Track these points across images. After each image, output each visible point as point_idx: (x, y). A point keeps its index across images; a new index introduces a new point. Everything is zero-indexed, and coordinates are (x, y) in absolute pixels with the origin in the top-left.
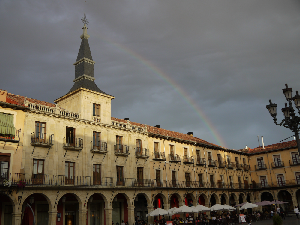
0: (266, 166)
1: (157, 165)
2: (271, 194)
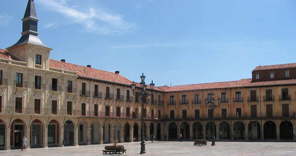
0: (176, 102)
2: (176, 124)
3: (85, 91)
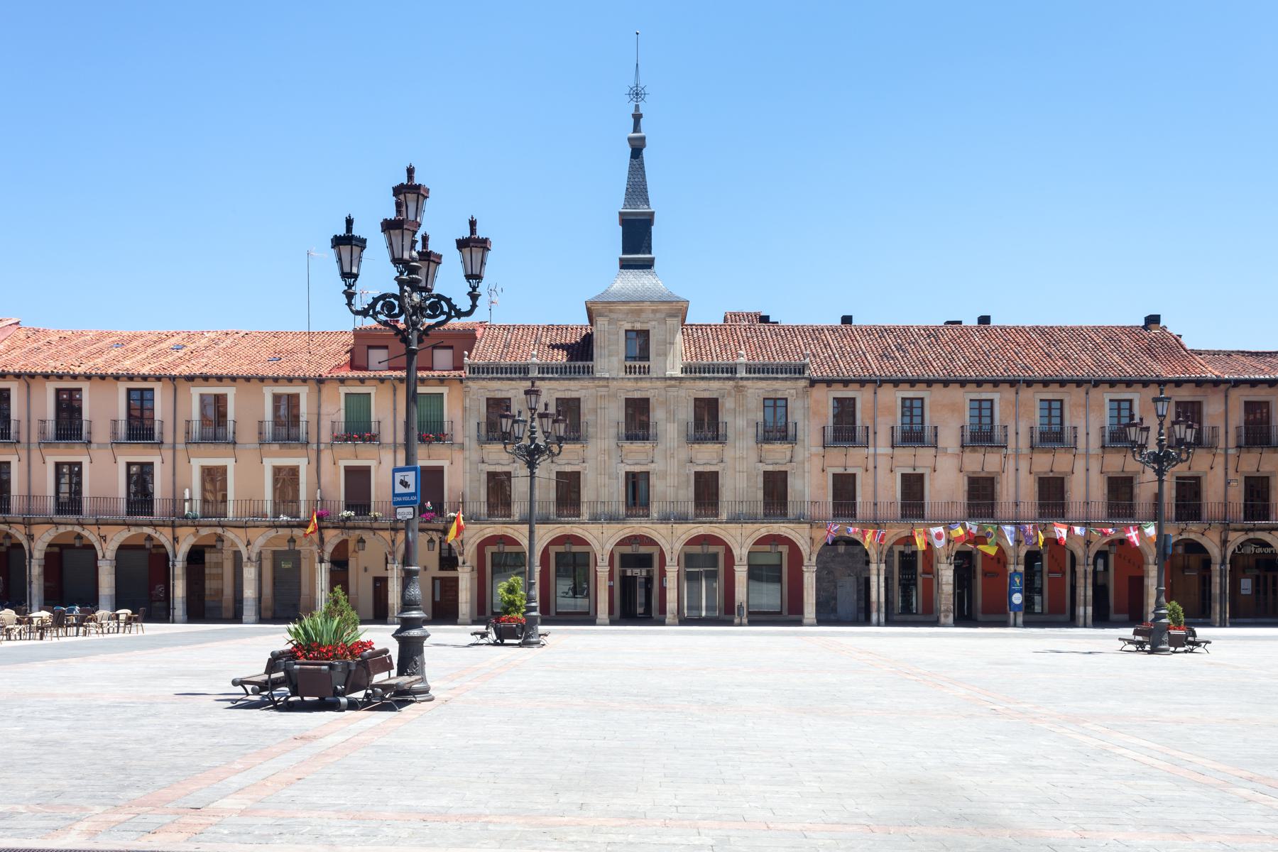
1: (1044, 463)
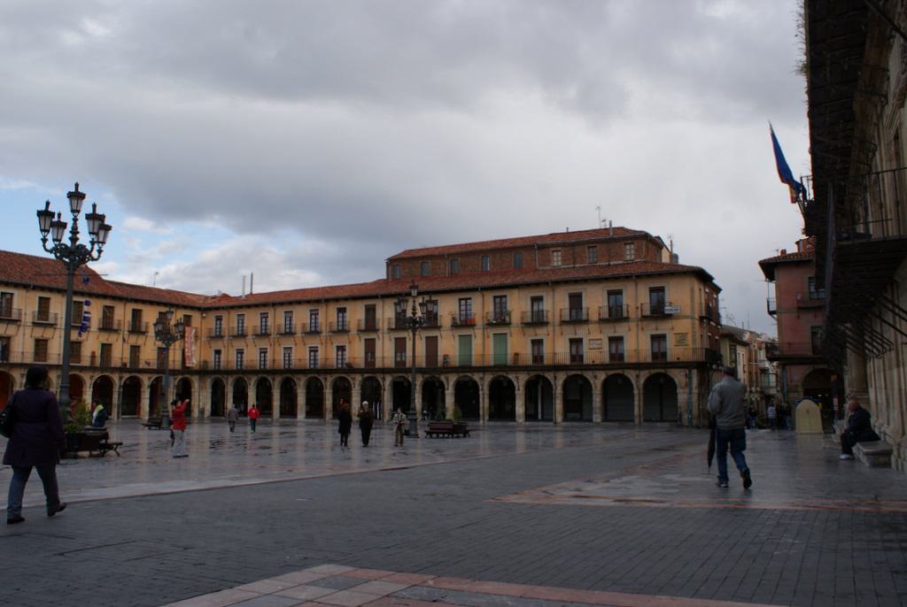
3: (11, 308)
